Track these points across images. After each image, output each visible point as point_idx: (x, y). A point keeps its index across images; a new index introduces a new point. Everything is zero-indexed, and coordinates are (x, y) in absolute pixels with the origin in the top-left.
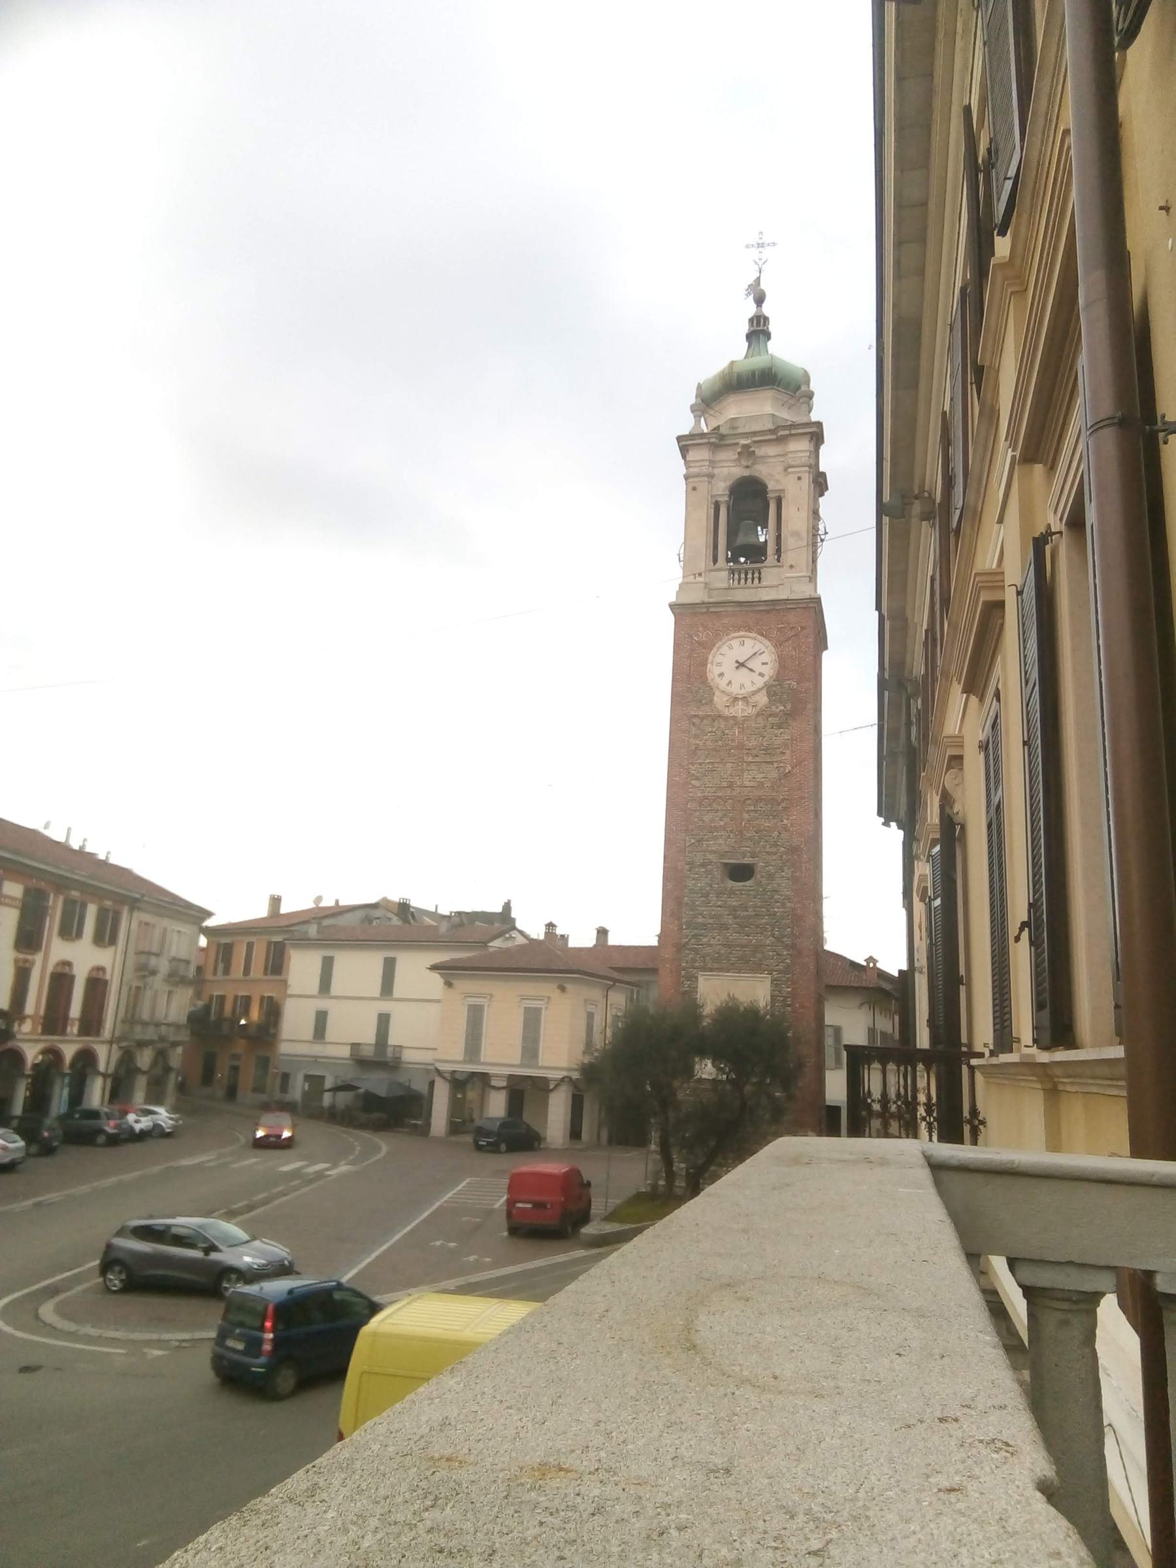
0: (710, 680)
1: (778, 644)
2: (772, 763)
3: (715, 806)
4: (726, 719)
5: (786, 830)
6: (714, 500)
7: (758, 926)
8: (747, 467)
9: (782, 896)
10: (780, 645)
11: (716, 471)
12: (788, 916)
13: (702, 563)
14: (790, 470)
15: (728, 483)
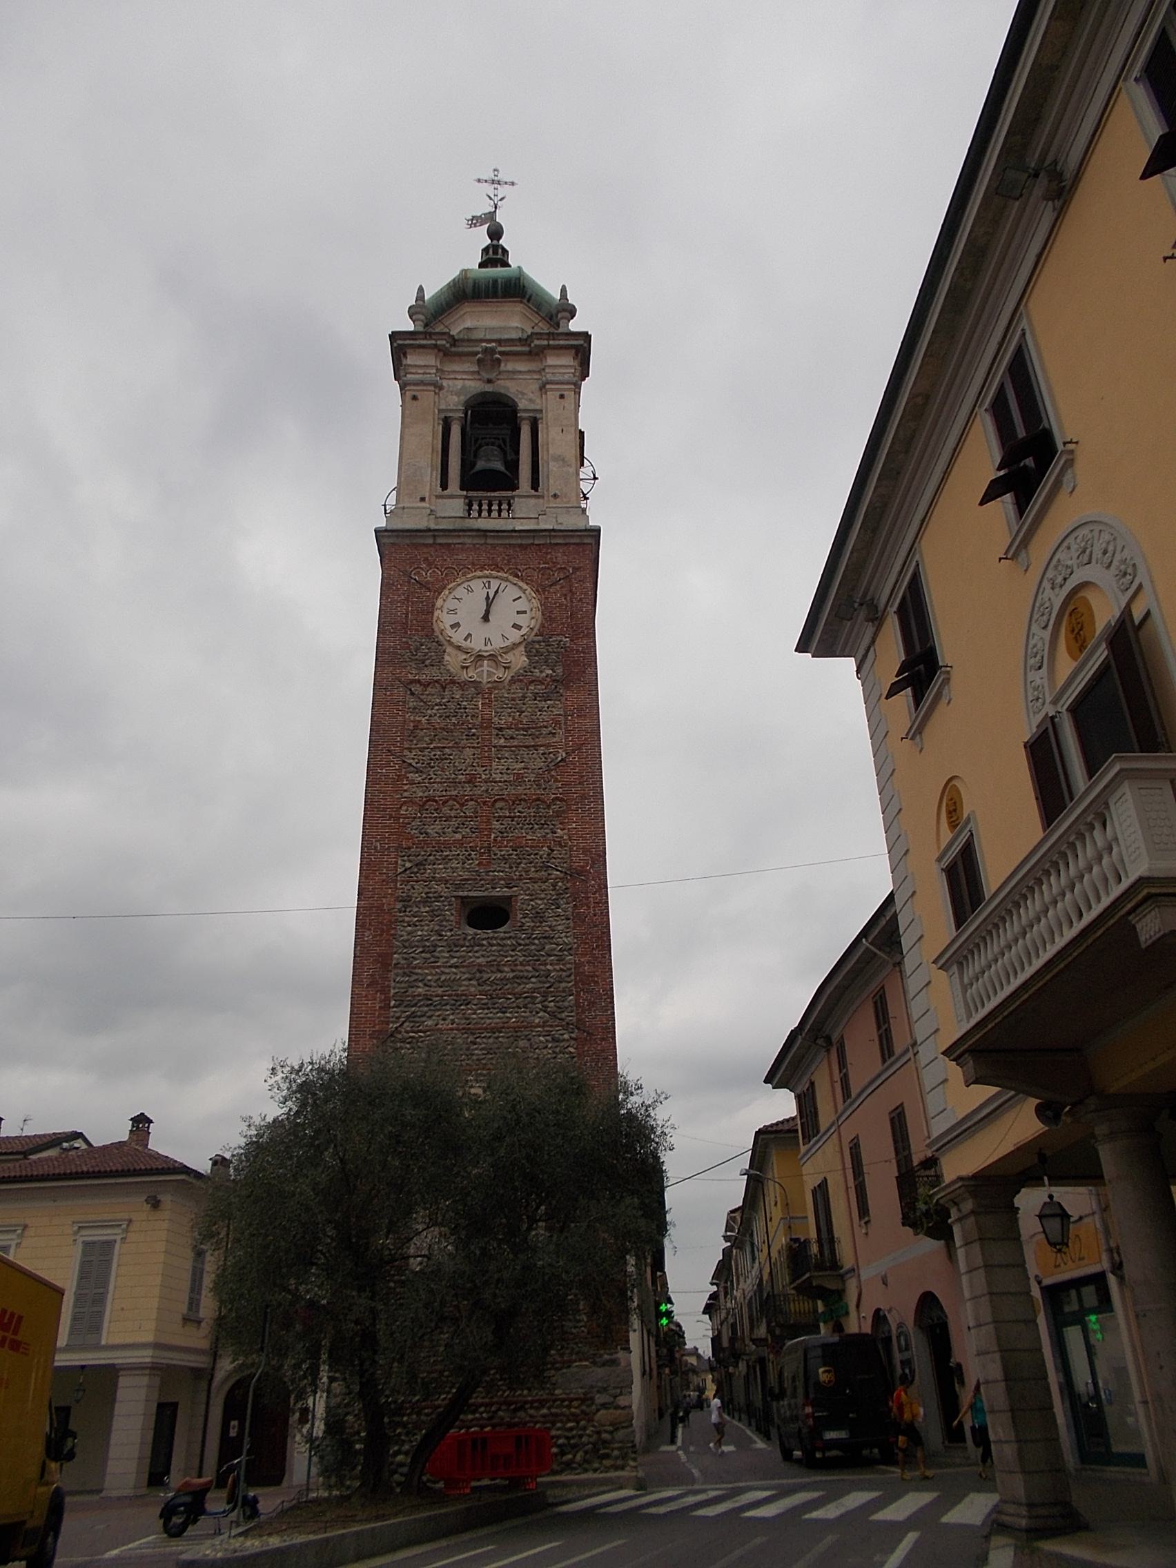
0: (437, 633)
1: (540, 589)
2: (536, 747)
3: (446, 810)
4: (463, 685)
5: (561, 846)
6: (443, 416)
7: (518, 996)
8: (489, 381)
9: (558, 945)
10: (544, 590)
11: (445, 383)
12: (570, 976)
13: (430, 478)
14: (548, 386)
15: (463, 398)
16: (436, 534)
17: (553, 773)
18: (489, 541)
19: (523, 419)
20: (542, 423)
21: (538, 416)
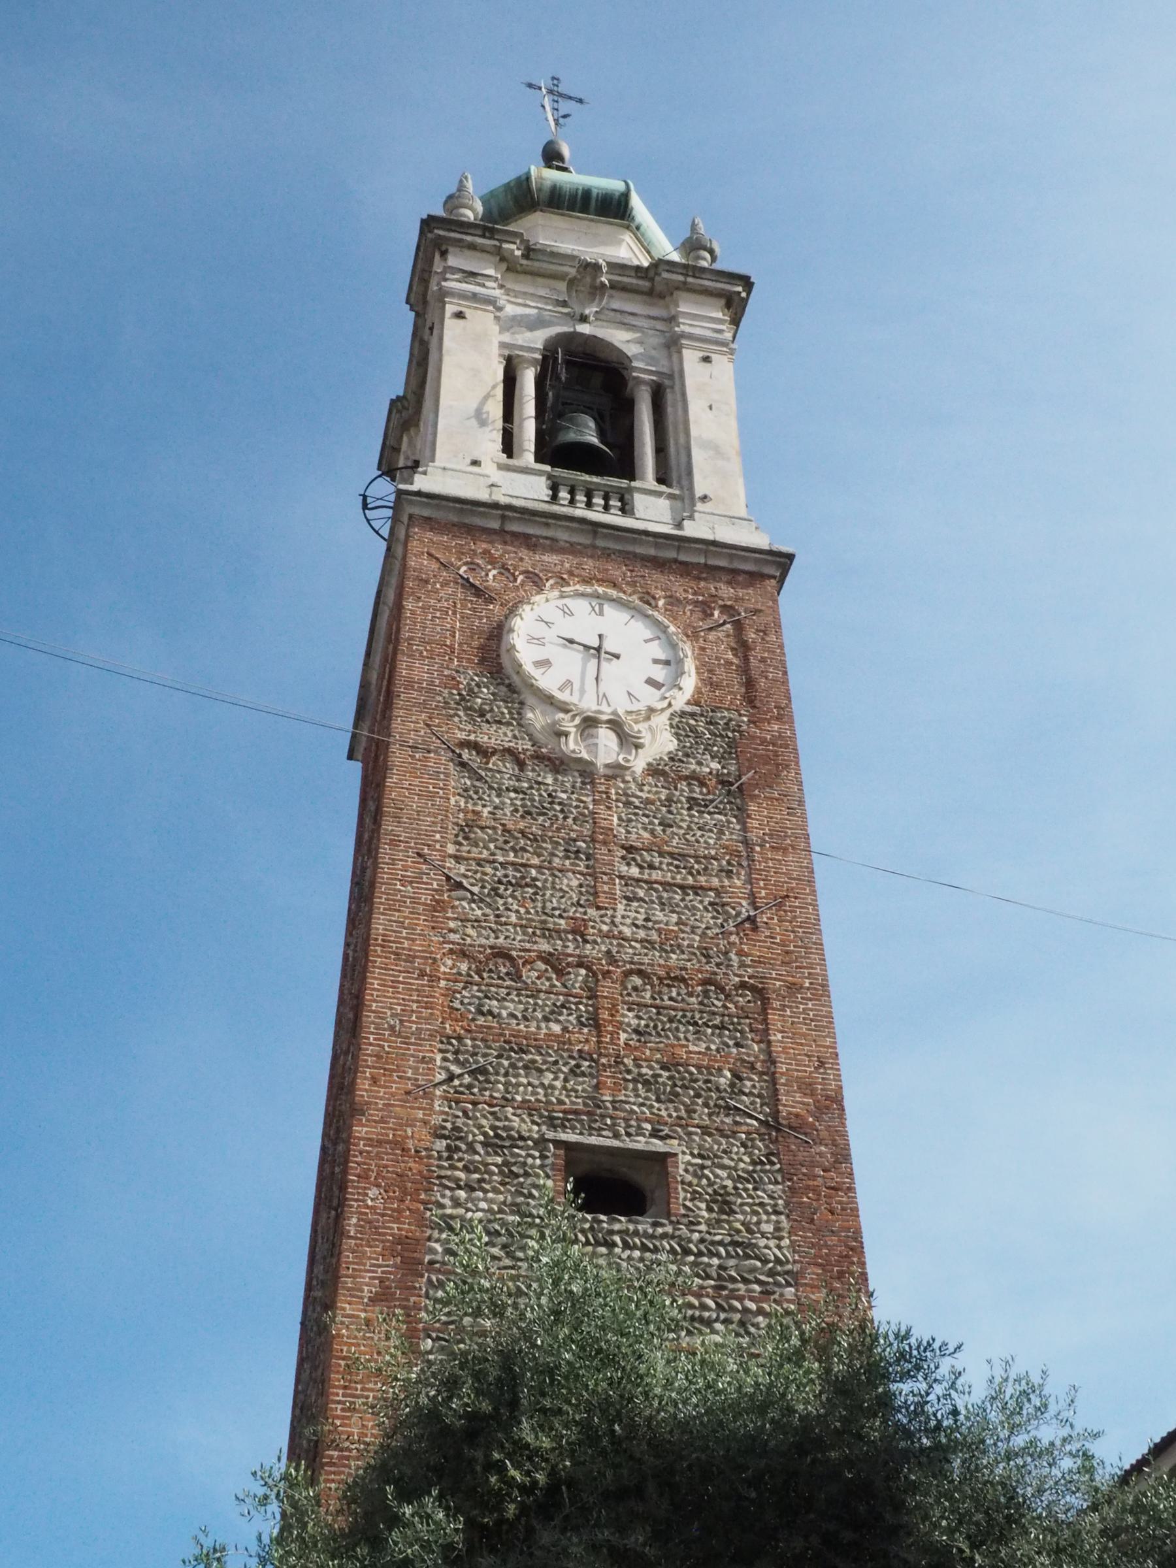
6: (507, 353)
16: (507, 513)
17: (733, 938)
18: (600, 543)
19: (639, 381)
20: (673, 392)
21: (667, 382)
